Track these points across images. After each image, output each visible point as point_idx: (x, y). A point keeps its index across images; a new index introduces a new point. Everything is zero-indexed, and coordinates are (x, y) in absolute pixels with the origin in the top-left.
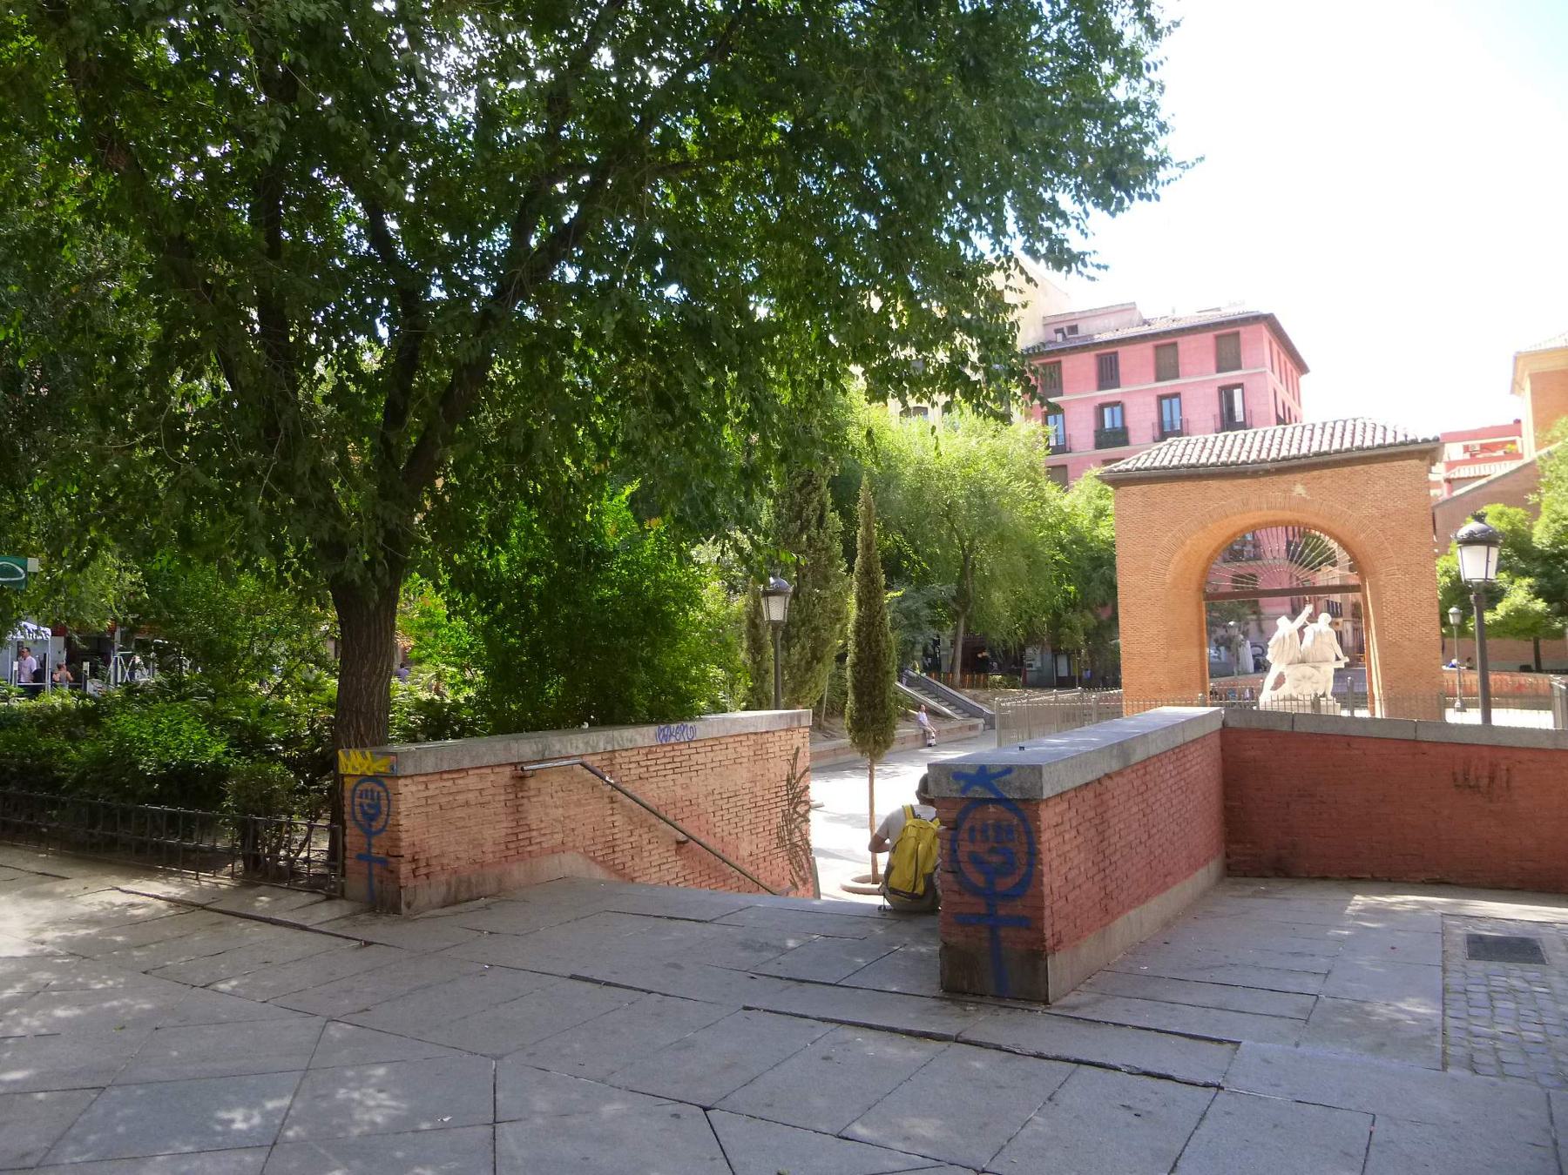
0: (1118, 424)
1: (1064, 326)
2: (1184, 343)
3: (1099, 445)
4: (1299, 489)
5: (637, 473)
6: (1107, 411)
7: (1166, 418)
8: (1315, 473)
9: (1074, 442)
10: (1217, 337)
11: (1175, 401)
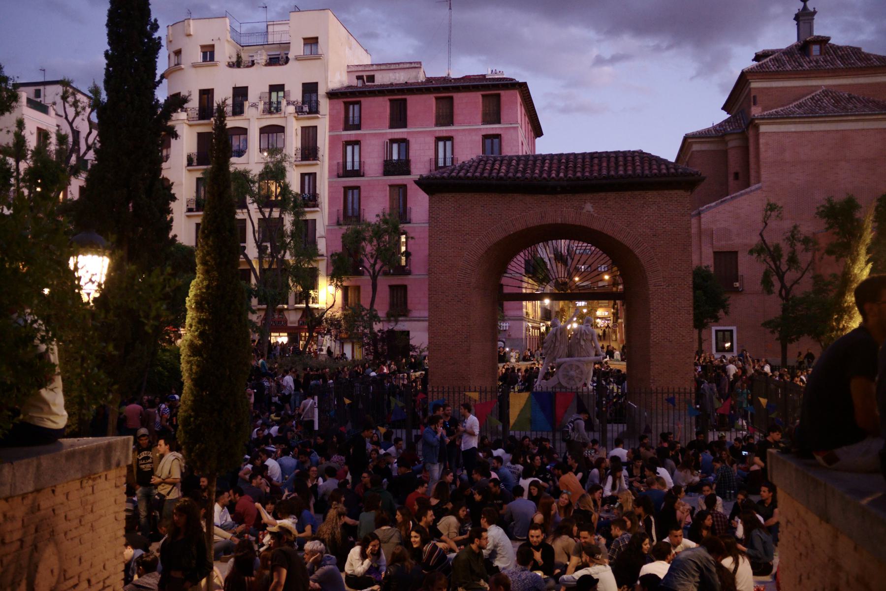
0: (403, 157)
1: (365, 74)
2: (460, 99)
3: (386, 173)
4: (589, 207)
5: (201, 356)
9: (367, 168)
10: (373, 81)
11: (449, 144)
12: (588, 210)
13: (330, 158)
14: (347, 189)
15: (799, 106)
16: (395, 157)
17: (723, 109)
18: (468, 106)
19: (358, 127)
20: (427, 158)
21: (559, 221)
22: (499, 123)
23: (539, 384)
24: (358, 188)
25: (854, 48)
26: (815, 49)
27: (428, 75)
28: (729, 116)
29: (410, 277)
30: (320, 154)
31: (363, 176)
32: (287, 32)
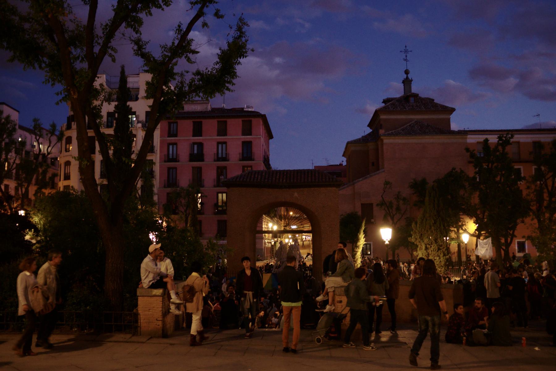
4: (296, 194)
11: (224, 145)
12: (296, 195)
13: (161, 152)
14: (169, 169)
15: (403, 130)
16: (196, 152)
17: (368, 126)
18: (234, 125)
19: (176, 135)
21: (283, 200)
22: (251, 135)
23: (274, 270)
24: (176, 168)
25: (430, 99)
26: (412, 100)
27: (213, 107)
28: (371, 130)
29: (203, 216)
30: (155, 149)
31: (178, 162)
32: (137, 82)
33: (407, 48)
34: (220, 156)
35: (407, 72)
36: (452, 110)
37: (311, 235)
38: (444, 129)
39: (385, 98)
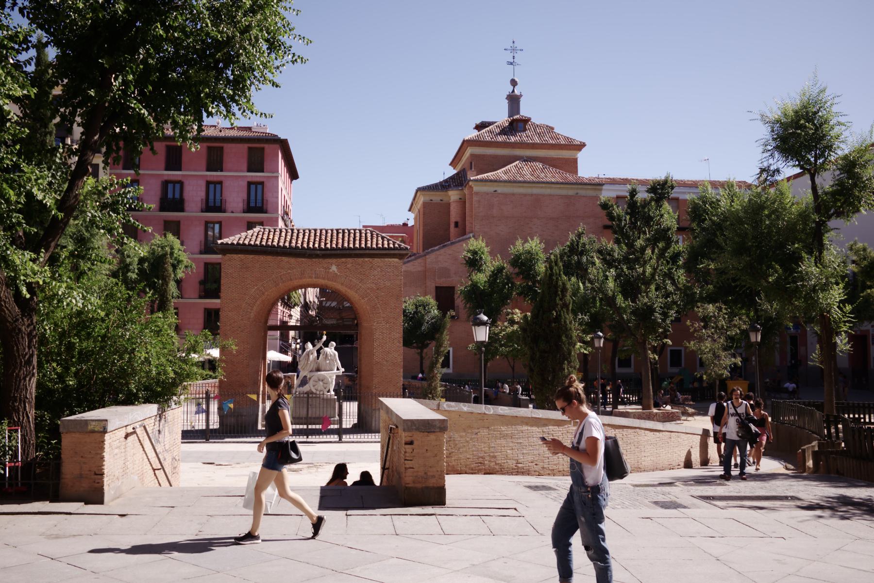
4: (334, 268)
6: (170, 186)
7: (211, 197)
8: (343, 260)
10: (250, 148)
11: (218, 186)
17: (451, 164)
20: (199, 199)
33: (515, 45)
34: (252, 204)
35: (514, 83)
36: (581, 146)
37: (204, 428)
38: (571, 165)
39: (478, 122)
